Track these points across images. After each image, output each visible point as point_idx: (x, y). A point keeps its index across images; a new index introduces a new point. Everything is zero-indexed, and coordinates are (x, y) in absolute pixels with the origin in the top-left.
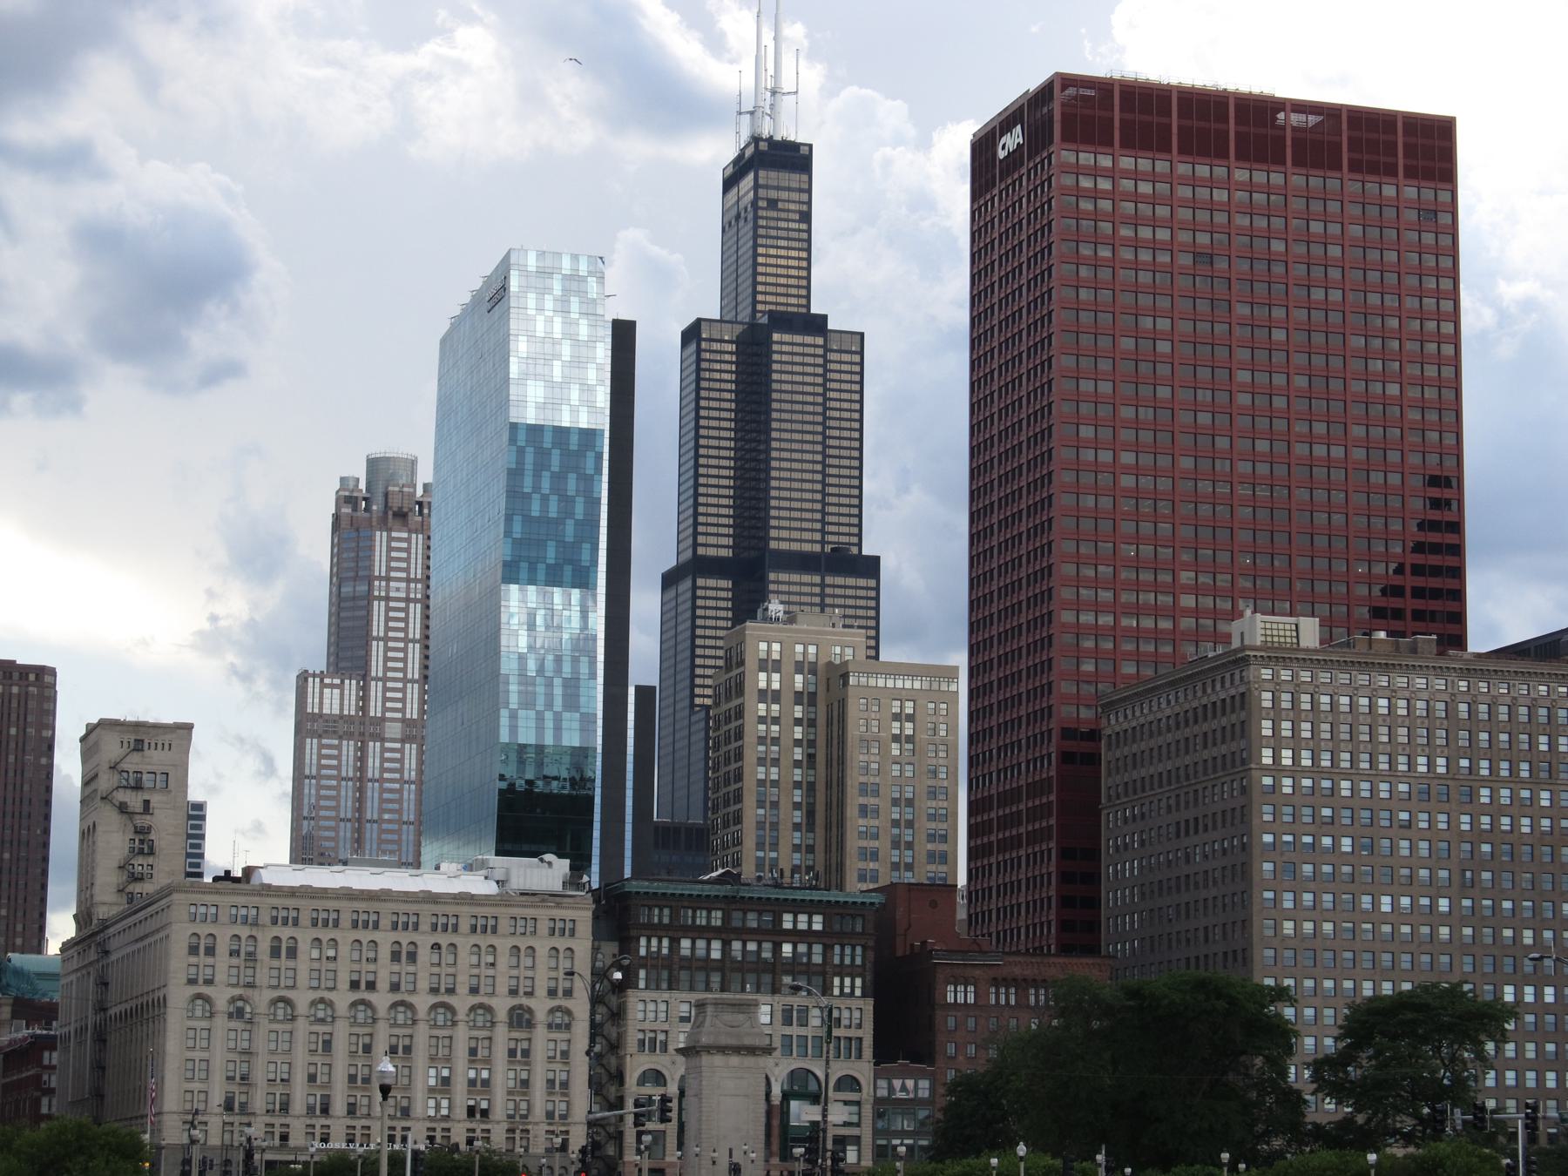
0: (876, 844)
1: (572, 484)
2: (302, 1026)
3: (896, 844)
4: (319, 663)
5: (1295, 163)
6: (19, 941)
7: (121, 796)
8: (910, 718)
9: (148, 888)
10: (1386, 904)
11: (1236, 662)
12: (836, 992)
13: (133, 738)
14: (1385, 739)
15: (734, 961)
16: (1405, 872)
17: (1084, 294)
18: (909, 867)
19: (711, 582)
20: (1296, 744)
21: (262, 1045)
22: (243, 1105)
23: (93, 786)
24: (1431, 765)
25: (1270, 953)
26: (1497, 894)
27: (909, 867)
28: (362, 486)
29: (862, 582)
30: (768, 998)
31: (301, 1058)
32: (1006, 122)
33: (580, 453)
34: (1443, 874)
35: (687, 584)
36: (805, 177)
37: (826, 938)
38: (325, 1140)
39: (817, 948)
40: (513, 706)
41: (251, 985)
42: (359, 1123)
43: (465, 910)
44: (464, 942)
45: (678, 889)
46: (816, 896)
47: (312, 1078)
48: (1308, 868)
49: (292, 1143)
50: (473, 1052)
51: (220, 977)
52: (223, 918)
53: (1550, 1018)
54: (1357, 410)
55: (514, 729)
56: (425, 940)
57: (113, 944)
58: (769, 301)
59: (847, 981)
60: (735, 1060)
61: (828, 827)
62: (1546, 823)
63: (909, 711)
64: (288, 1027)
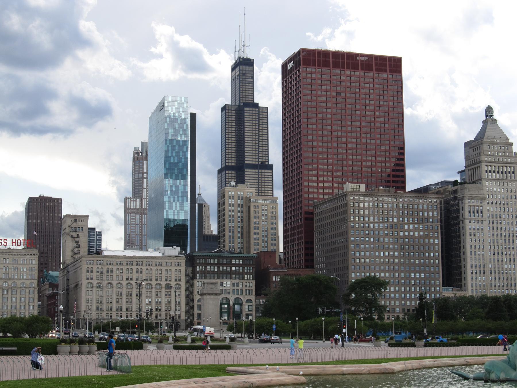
0: (258, 241)
1: (181, 154)
2: (115, 289)
3: (263, 241)
4: (130, 195)
5: (362, 69)
6: (54, 268)
7: (72, 233)
8: (266, 210)
9: (78, 256)
10: (382, 254)
11: (344, 195)
12: (246, 278)
13: (74, 219)
14: (381, 213)
15: (221, 272)
16: (387, 246)
17: (309, 103)
18: (267, 247)
19: (230, 172)
20: (359, 215)
21: (105, 293)
22: (101, 309)
23: (65, 231)
24: (393, 220)
25: (353, 267)
26: (409, 251)
27: (267, 247)
28: (140, 149)
29: (269, 171)
30: (229, 280)
31: (115, 297)
32: (290, 60)
33: (183, 146)
34: (396, 246)
35: (224, 172)
36: (252, 68)
37: (243, 265)
38: (121, 317)
39: (241, 268)
40: (167, 209)
41: (102, 280)
42: (129, 313)
43: (154, 261)
44: (154, 268)
45: (208, 254)
46: (240, 255)
47: (117, 302)
48: (362, 246)
49: (113, 318)
50: (157, 295)
51: (95, 278)
52: (95, 263)
53: (423, 281)
54: (378, 131)
55: (167, 215)
56: (144, 268)
57: (70, 270)
58: (245, 100)
59: (249, 276)
60: (212, 297)
61: (246, 238)
62: (421, 233)
63: (266, 208)
64: (111, 290)
